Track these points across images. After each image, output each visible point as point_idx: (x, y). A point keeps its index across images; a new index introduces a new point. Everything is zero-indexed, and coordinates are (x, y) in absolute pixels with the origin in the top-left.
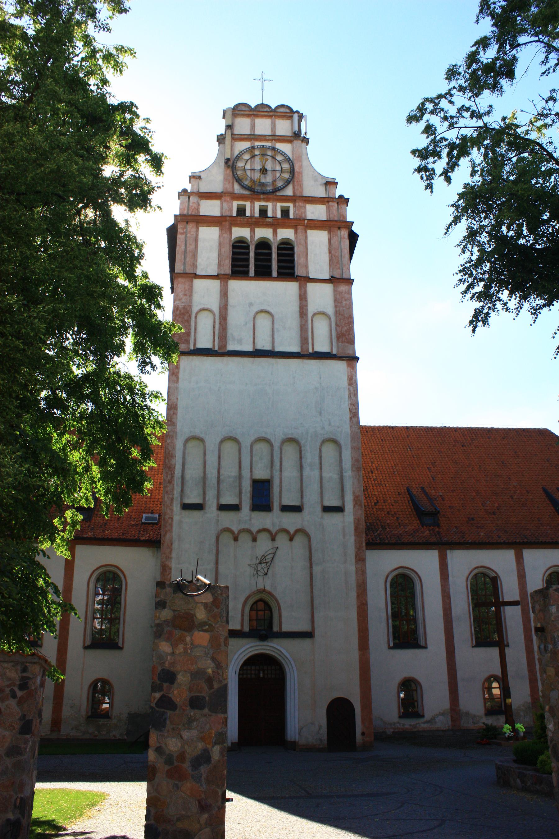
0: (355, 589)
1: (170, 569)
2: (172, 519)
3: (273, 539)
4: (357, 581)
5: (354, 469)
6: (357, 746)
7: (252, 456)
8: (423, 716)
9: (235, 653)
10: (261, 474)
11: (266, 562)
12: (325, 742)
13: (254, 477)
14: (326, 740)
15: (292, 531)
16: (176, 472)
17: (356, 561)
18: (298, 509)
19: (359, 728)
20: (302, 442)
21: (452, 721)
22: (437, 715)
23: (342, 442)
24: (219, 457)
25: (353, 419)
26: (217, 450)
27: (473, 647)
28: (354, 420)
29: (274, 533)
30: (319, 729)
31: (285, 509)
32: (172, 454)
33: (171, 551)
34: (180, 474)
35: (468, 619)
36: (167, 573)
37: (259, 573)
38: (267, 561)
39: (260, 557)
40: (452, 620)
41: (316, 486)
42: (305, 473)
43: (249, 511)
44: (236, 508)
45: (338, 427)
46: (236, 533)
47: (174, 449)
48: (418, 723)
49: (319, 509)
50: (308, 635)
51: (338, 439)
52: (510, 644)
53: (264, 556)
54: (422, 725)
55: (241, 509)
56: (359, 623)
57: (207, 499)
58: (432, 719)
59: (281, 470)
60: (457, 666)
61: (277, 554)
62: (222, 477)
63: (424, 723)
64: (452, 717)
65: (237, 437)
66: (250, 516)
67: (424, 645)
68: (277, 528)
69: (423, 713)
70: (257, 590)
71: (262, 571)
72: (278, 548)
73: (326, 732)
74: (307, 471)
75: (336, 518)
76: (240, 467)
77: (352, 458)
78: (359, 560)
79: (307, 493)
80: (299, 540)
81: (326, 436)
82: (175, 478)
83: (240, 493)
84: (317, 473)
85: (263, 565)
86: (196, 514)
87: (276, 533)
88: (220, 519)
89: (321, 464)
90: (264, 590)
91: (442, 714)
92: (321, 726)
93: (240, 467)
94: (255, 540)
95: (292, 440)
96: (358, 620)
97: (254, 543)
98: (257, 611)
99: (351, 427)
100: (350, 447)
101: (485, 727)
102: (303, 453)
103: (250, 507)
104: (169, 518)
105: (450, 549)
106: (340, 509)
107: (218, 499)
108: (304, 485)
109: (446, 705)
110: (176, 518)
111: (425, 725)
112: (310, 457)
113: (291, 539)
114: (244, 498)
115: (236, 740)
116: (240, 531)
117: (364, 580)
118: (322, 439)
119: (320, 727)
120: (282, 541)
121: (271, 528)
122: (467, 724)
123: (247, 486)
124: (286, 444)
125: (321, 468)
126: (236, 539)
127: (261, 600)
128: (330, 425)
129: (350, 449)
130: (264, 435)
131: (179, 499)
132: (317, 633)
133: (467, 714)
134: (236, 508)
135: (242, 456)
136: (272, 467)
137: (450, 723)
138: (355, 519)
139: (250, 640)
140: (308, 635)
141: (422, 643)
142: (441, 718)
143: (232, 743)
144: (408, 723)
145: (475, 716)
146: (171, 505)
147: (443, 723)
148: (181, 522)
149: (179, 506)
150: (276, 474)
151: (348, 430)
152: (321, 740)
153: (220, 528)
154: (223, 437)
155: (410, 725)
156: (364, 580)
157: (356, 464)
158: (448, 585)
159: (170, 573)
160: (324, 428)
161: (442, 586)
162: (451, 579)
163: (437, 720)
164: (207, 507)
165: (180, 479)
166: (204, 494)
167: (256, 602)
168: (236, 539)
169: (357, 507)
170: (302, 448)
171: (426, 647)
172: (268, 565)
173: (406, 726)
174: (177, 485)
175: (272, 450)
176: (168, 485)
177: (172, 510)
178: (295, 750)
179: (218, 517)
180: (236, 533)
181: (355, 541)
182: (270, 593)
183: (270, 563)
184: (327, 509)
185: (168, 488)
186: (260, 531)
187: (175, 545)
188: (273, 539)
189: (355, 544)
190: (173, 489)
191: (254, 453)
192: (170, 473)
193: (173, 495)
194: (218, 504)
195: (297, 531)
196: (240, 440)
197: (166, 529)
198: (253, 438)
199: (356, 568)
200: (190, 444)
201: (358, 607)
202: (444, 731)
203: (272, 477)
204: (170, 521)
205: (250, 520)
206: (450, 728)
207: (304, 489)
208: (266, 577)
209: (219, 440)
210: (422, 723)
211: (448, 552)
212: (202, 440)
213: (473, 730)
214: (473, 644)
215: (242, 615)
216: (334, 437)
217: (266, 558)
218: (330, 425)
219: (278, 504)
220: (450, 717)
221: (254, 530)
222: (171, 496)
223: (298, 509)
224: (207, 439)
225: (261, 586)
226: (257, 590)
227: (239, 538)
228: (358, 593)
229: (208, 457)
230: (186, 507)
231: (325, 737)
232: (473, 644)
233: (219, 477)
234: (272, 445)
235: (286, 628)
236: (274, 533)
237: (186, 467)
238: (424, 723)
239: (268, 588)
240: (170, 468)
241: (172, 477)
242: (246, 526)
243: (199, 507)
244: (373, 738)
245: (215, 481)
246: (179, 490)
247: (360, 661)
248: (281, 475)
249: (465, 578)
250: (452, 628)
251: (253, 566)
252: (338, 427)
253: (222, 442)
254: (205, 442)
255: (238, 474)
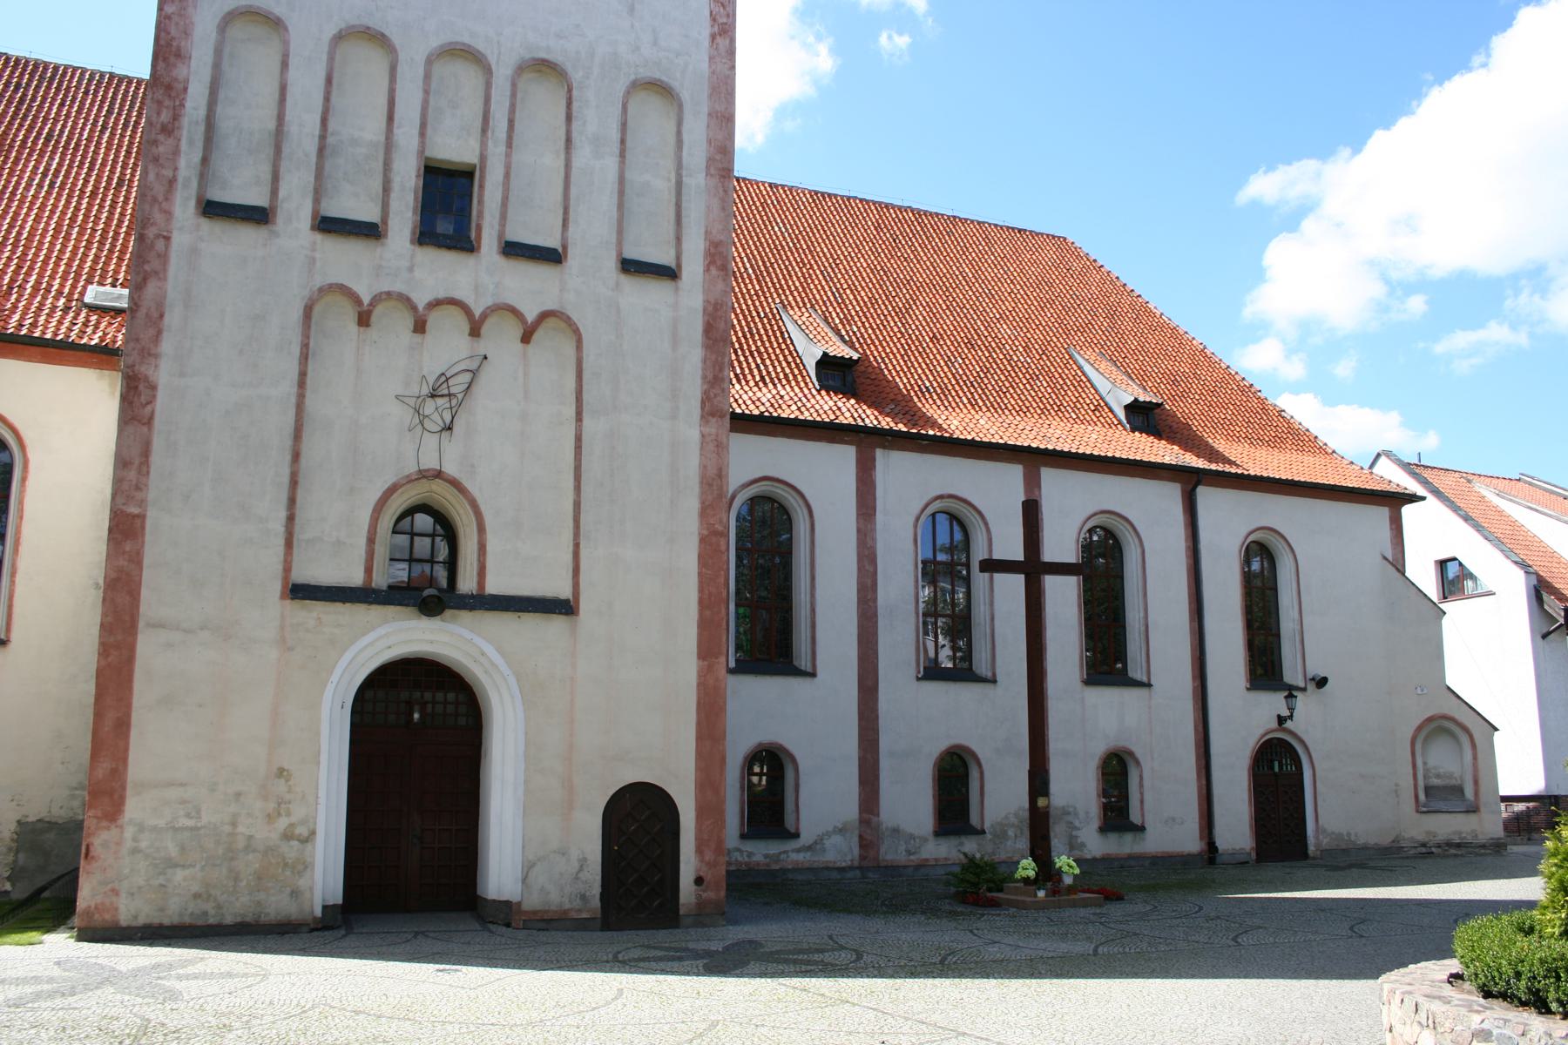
0: (697, 490)
1: (153, 388)
2: (167, 239)
3: (475, 332)
4: (704, 468)
5: (712, 171)
6: (682, 912)
7: (427, 92)
8: (796, 835)
9: (345, 650)
10: (455, 149)
11: (450, 395)
12: (596, 903)
13: (428, 153)
14: (598, 896)
15: (530, 317)
16: (189, 104)
17: (702, 417)
18: (551, 257)
19: (689, 864)
20: (576, 76)
21: (861, 846)
22: (828, 834)
23: (685, 96)
24: (329, 81)
25: (719, 40)
26: (325, 57)
27: (918, 679)
28: (722, 42)
29: (477, 313)
30: (581, 869)
31: (513, 250)
32: (179, 48)
33: (159, 333)
34: (202, 112)
35: (914, 615)
36: (143, 399)
37: (427, 423)
38: (453, 390)
39: (431, 380)
40: (875, 615)
41: (606, 201)
42: (577, 162)
43: (408, 245)
44: (370, 231)
45: (678, 55)
46: (366, 300)
47: (187, 33)
48: (784, 852)
49: (611, 264)
50: (563, 608)
51: (675, 84)
52: (999, 678)
53: (444, 378)
54: (794, 856)
55: (385, 236)
56: (701, 583)
57: (282, 193)
58: (816, 843)
59: (509, 144)
60: (880, 721)
61: (483, 378)
62: (330, 140)
63: (798, 851)
64: (861, 837)
65: (387, 33)
66: (413, 256)
67: (809, 669)
68: (489, 302)
69: (797, 829)
70: (420, 471)
71: (436, 417)
72: (486, 358)
73: (599, 878)
74: (583, 156)
75: (653, 292)
76: (390, 118)
77: (709, 142)
78: (713, 415)
79: (579, 212)
80: (549, 341)
81: (645, 73)
82: (185, 121)
83: (386, 189)
84: (611, 164)
85: (440, 401)
86: (247, 235)
87: (484, 316)
88: (318, 255)
89: (623, 141)
90: (439, 475)
91: (841, 831)
92: (585, 859)
93: (390, 118)
94: (420, 327)
95: (544, 67)
96: (700, 574)
97: (418, 338)
98: (413, 534)
99: (711, 58)
100: (705, 109)
101: (965, 861)
102: (575, 105)
103: (413, 233)
104: (158, 236)
105: (884, 447)
106: (668, 273)
107: (317, 201)
108: (573, 191)
109: (849, 809)
110: (180, 240)
111: (800, 857)
112: (598, 119)
113: (526, 338)
114: (394, 205)
115: (339, 900)
116: (377, 299)
117: (720, 470)
118: (633, 77)
119: (583, 862)
120: (501, 342)
121: (469, 300)
122: (892, 853)
123: (407, 177)
124: (526, 76)
125: (622, 154)
126: (364, 320)
127: (424, 508)
128: (655, 43)
129: (704, 118)
130: (466, 39)
131: (194, 184)
132: (584, 606)
133: (896, 831)
134: (370, 231)
135: (398, 87)
136: (485, 129)
137: (856, 851)
138: (707, 302)
139: (391, 610)
140: (563, 608)
141: (803, 662)
142: (837, 839)
143: (325, 908)
144: (761, 852)
145: (912, 837)
146: (167, 199)
147: (842, 851)
148: (194, 251)
149: (193, 203)
150: (496, 151)
151: (704, 66)
152: (583, 897)
153: (319, 281)
154: (343, 26)
155: (766, 856)
156: (720, 470)
157: (718, 157)
158: (874, 530)
159: (151, 401)
160: (638, 48)
161: (859, 531)
162: (879, 517)
163: (827, 843)
164: (280, 218)
165: (202, 128)
166: (276, 178)
167: (411, 512)
168: (364, 320)
169: (714, 271)
170: (575, 93)
171: (813, 675)
172: (454, 402)
173: (758, 858)
174: (191, 142)
175: (488, 86)
176: (161, 138)
177: (168, 214)
178: (508, 925)
179: (314, 250)
180: (366, 300)
181: (704, 361)
182: (455, 483)
183: (460, 396)
184: (631, 267)
185: (161, 149)
186: (436, 304)
187: (172, 319)
188: (475, 332)
189: (704, 369)
190: (176, 152)
191: (434, 85)
192: (167, 102)
193: (176, 169)
194: (315, 213)
195: (544, 316)
196: (396, 41)
197: (147, 267)
198: (435, 42)
199: (703, 436)
200: (237, 31)
201: (703, 540)
202: (842, 870)
203: (483, 158)
204: (160, 245)
205: (411, 269)
206: (856, 864)
207: (572, 202)
208: (445, 434)
209: (330, 31)
210: (793, 851)
211: (879, 453)
212: (275, 24)
213: (905, 867)
214: (919, 672)
215: (371, 540)
216: (664, 78)
217: (451, 382)
218: (655, 43)
219: (495, 234)
220: (856, 839)
221: (421, 300)
222: (168, 173)
223: (551, 257)
224: (295, 23)
225: (430, 463)
226: (420, 471)
227: (374, 318)
228: (703, 503)
229: (293, 74)
230: (213, 210)
231: (596, 890)
232: (919, 672)
233: (323, 138)
234: (488, 71)
235: (496, 585)
236: (477, 313)
237: (221, 95)
238: (798, 851)
239: (450, 469)
240: (169, 87)
241: (176, 117)
242: (398, 287)
243: (258, 216)
244: (723, 893)
245: (311, 147)
246: (197, 157)
247: (699, 685)
248: (508, 155)
249: (912, 520)
250: (875, 634)
251: (412, 402)
252: (678, 55)
253: (339, 38)
254: (286, 29)
255: (383, 138)
